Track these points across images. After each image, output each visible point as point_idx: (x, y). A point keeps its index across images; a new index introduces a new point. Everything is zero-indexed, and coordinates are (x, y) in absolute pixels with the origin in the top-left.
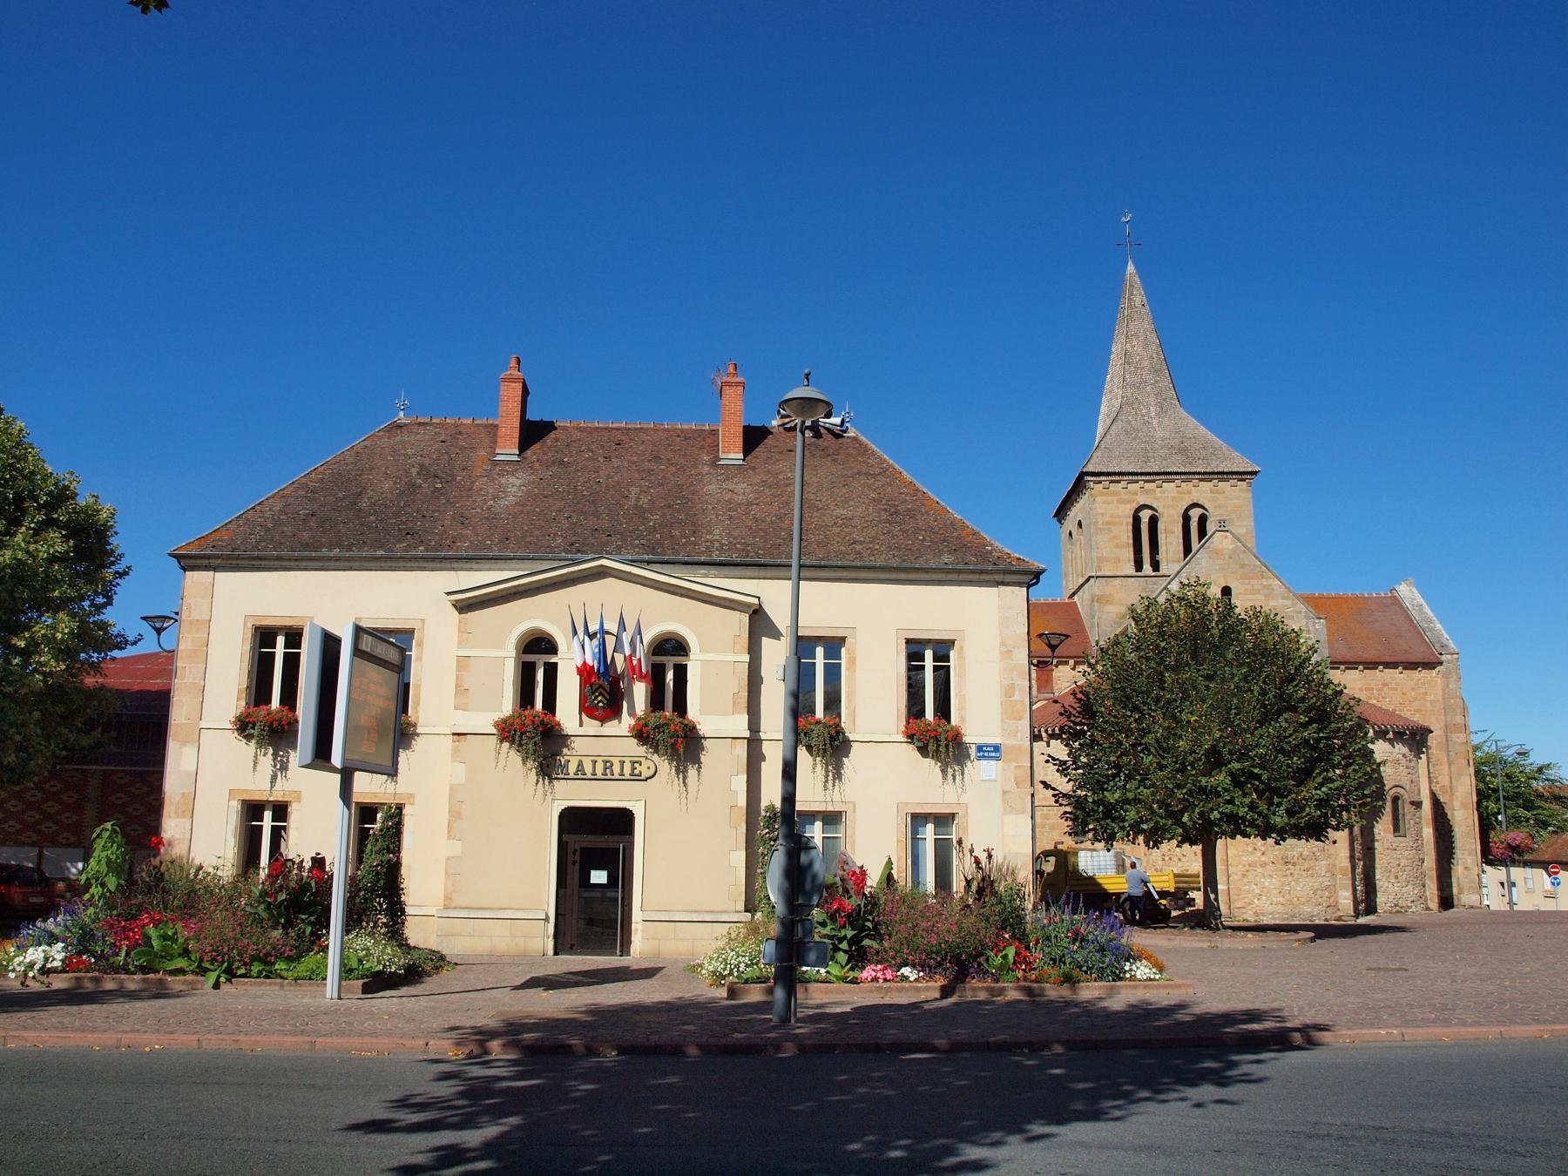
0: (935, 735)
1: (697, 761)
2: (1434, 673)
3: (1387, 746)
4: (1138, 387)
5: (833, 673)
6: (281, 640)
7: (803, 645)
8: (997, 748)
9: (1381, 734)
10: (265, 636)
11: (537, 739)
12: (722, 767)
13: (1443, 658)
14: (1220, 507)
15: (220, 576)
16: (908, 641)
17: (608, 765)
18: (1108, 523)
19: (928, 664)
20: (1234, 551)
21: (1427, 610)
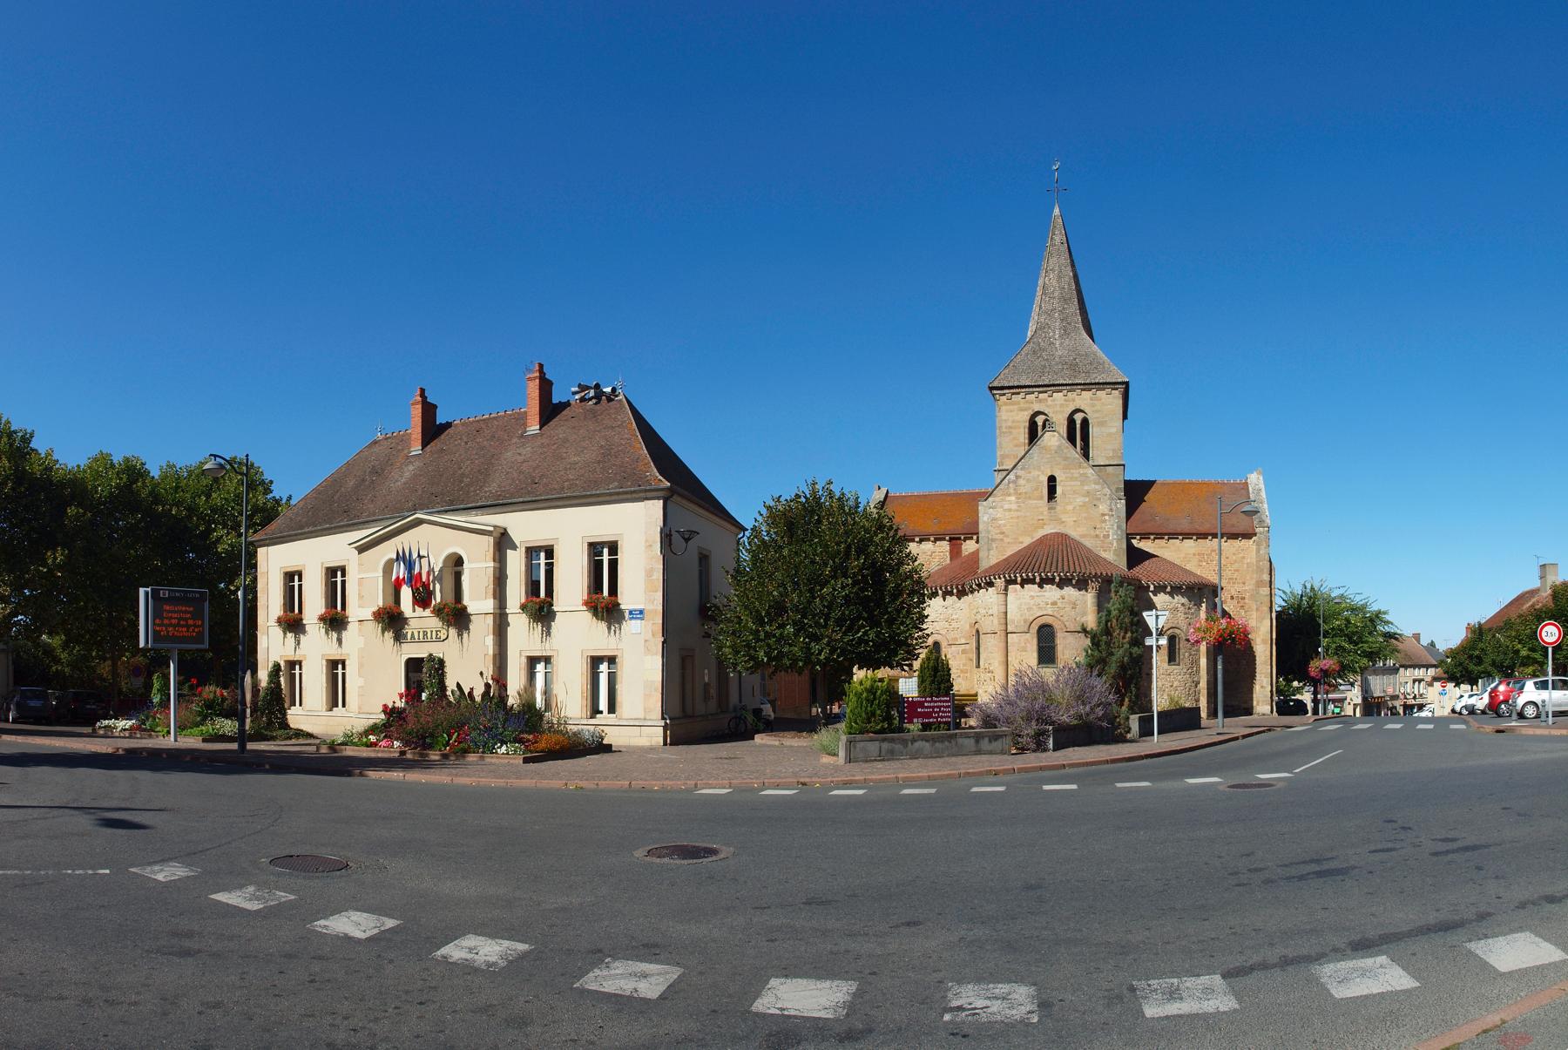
0: (606, 609)
1: (467, 629)
3: (1167, 597)
4: (1049, 314)
5: (614, 565)
6: (606, 551)
7: (531, 552)
8: (641, 612)
9: (1160, 589)
10: (595, 548)
11: (391, 620)
16: (590, 544)
17: (425, 633)
19: (603, 560)
21: (1263, 494)
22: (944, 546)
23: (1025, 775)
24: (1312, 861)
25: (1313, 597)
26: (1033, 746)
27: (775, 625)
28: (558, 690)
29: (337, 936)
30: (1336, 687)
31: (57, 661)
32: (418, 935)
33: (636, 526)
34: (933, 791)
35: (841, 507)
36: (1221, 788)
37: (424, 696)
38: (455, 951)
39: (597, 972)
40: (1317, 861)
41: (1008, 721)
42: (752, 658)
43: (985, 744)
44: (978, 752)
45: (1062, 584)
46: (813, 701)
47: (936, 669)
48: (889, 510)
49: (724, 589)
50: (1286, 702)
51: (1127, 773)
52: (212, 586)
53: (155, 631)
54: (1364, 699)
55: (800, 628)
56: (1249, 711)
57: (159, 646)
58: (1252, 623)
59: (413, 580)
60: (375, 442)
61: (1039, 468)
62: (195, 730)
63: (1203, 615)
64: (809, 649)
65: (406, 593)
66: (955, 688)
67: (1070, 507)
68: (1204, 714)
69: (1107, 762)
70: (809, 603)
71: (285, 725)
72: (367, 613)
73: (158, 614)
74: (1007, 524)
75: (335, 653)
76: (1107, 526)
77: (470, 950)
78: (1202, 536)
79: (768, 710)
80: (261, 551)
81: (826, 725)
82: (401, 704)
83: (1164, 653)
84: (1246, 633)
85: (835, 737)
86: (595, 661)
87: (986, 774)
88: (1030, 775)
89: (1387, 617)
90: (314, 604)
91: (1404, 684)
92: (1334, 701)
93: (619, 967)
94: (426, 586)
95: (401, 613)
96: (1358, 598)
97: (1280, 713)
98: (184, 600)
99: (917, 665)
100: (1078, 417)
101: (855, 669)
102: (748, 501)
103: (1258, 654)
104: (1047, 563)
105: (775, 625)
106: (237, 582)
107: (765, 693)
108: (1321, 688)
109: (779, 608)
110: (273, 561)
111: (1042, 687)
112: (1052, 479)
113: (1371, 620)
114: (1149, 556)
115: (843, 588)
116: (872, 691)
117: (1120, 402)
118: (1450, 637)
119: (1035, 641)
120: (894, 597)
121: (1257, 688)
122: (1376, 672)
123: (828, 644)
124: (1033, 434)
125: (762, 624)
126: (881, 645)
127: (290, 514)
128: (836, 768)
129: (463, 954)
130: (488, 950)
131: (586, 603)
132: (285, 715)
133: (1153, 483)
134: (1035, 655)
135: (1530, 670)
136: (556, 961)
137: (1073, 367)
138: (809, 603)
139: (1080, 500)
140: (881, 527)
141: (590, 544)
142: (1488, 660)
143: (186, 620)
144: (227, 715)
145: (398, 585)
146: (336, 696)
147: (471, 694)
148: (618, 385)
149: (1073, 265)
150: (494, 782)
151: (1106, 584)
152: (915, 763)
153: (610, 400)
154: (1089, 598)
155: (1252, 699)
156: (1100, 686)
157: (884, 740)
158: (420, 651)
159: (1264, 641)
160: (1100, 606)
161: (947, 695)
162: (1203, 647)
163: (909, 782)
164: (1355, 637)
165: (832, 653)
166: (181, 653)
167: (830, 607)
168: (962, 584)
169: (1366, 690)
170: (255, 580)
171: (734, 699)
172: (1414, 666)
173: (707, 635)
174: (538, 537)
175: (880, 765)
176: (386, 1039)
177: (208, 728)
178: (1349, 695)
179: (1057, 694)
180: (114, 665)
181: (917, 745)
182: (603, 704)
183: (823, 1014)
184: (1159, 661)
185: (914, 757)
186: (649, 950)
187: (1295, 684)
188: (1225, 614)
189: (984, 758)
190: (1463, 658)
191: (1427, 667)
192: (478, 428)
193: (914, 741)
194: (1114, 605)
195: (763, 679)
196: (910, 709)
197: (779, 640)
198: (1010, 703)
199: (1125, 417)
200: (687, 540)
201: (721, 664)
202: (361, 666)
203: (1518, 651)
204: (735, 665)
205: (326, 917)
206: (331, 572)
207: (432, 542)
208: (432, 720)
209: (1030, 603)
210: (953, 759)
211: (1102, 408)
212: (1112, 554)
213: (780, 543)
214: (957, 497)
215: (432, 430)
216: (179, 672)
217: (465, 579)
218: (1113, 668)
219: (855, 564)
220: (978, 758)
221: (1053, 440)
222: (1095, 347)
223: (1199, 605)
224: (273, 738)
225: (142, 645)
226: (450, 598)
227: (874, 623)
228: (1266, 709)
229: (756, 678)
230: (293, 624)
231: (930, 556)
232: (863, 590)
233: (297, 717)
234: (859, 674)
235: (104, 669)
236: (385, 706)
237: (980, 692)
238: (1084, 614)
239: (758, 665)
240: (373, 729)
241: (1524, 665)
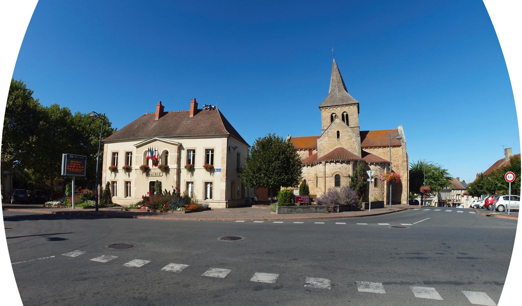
0: (210, 168)
1: (169, 173)
3: (374, 166)
4: (335, 86)
5: (212, 156)
7: (189, 151)
8: (220, 169)
9: (372, 164)
10: (207, 151)
11: (145, 169)
12: (173, 173)
15: (109, 144)
16: (206, 150)
17: (156, 174)
19: (209, 154)
21: (403, 132)
22: (307, 152)
23: (330, 219)
24: (416, 253)
25: (421, 165)
26: (333, 211)
28: (195, 191)
29: (132, 267)
30: (429, 196)
31: (30, 179)
32: (156, 264)
33: (220, 145)
36: (389, 227)
37: (155, 193)
38: (167, 268)
39: (208, 271)
40: (417, 254)
41: (325, 203)
42: (252, 183)
43: (318, 210)
44: (316, 212)
45: (342, 163)
46: (269, 196)
47: (304, 188)
48: (291, 142)
49: (244, 164)
50: (412, 200)
51: (359, 221)
52: (88, 155)
53: (67, 170)
54: (439, 201)
55: (265, 175)
57: (68, 175)
58: (401, 174)
59: (153, 157)
60: (145, 115)
62: (81, 205)
63: (385, 172)
65: (150, 161)
68: (385, 203)
71: (111, 202)
72: (138, 167)
73: (68, 163)
74: (326, 145)
75: (128, 179)
76: (355, 145)
77: (172, 267)
78: (384, 147)
79: (256, 198)
80: (105, 145)
81: (272, 203)
82: (148, 195)
83: (373, 183)
84: (399, 177)
85: (275, 207)
86: (206, 183)
87: (319, 218)
89: (447, 172)
90: (121, 163)
91: (453, 196)
92: (428, 201)
93: (214, 270)
94: (157, 159)
95: (149, 167)
96: (437, 165)
97: (410, 204)
98: (78, 159)
99: (299, 186)
100: (345, 114)
102: (251, 137)
103: (403, 184)
106: (97, 154)
107: (255, 194)
108: (424, 196)
109: (260, 169)
110: (109, 148)
111: (336, 193)
112: (338, 132)
113: (442, 173)
114: (368, 154)
116: (286, 193)
118: (470, 178)
119: (334, 180)
121: (403, 195)
122: (443, 191)
124: (332, 119)
125: (255, 173)
126: (289, 180)
127: (116, 134)
128: (275, 215)
129: (170, 269)
130: (177, 267)
131: (204, 167)
132: (111, 199)
134: (334, 184)
135: (501, 192)
136: (196, 269)
137: (342, 100)
139: (347, 138)
140: (289, 147)
141: (206, 150)
142: (485, 188)
143: (78, 166)
144: (92, 199)
145: (148, 159)
146: (127, 193)
147: (169, 193)
148: (216, 106)
150: (176, 219)
151: (355, 163)
152: (298, 214)
153: (213, 109)
154: (350, 167)
156: (354, 193)
158: (154, 179)
159: (405, 180)
160: (354, 169)
162: (385, 182)
163: (296, 220)
164: (436, 179)
165: (275, 182)
166: (76, 178)
167: (274, 169)
168: (313, 162)
169: (439, 197)
170: (103, 154)
171: (246, 195)
172: (457, 189)
174: (191, 147)
175: (288, 215)
176: (150, 294)
177: (85, 204)
178: (433, 199)
180: (52, 181)
181: (299, 209)
182: (208, 196)
183: (269, 282)
184: (371, 186)
185: (298, 213)
186: (222, 265)
187: (415, 194)
188: (392, 171)
189: (318, 214)
190: (475, 186)
191: (462, 190)
192: (175, 114)
193: (298, 208)
196: (297, 199)
197: (259, 179)
198: (326, 198)
199: (359, 113)
200: (234, 149)
201: (243, 185)
202: (136, 183)
203: (496, 184)
204: (247, 185)
205: (128, 262)
206: (128, 153)
207: (159, 146)
208: (158, 200)
209: (332, 168)
211: (352, 111)
212: (357, 153)
215: (162, 113)
216: (75, 184)
217: (169, 158)
218: (357, 188)
219: (281, 157)
220: (316, 214)
221: (338, 121)
222: (348, 94)
224: (107, 207)
225: (62, 174)
226: (164, 164)
227: (287, 174)
229: (253, 188)
230: (114, 169)
231: (303, 155)
232: (284, 164)
233: (115, 200)
234: (282, 189)
235: (48, 183)
236: (143, 196)
238: (349, 171)
239: (253, 185)
240: (139, 203)
241: (499, 190)
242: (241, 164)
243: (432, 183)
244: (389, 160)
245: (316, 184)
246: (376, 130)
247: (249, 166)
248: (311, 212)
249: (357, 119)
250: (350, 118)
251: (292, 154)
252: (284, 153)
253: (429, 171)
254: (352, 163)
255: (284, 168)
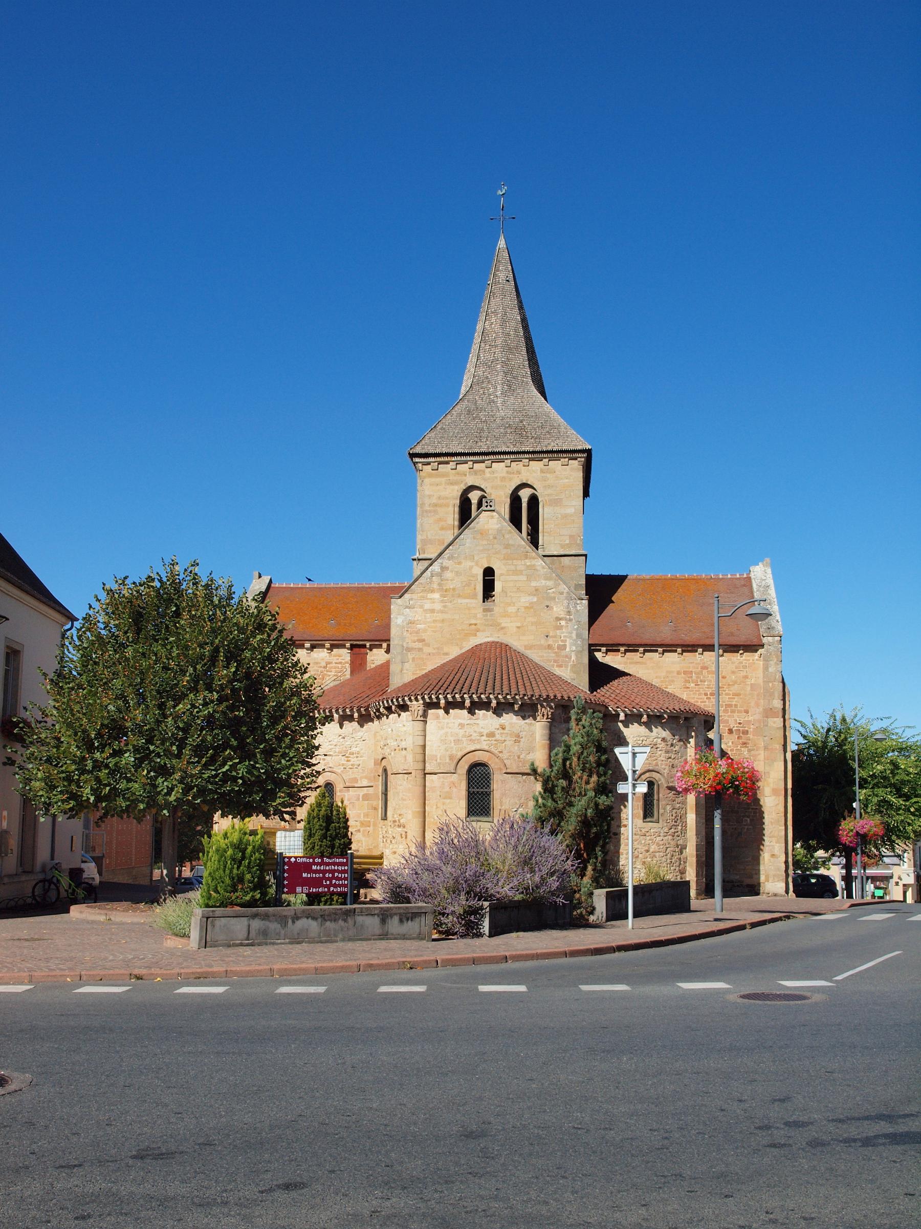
2: (757, 655)
3: (643, 730)
4: (490, 366)
9: (633, 718)
13: (765, 640)
14: (549, 487)
18: (436, 505)
20: (499, 531)
21: (772, 592)
22: (344, 655)
24: (880, 1117)
26: (458, 928)
27: (108, 751)
34: (321, 989)
35: (209, 597)
36: (733, 998)
40: (889, 1118)
41: (425, 894)
42: (73, 796)
43: (394, 925)
44: (384, 936)
45: (501, 709)
46: (157, 856)
47: (328, 819)
48: (271, 603)
55: (143, 756)
56: (753, 889)
58: (759, 766)
61: (472, 558)
64: (155, 786)
66: (353, 846)
67: (512, 609)
68: (693, 893)
69: (565, 954)
70: (158, 722)
74: (428, 628)
76: (563, 633)
78: (690, 648)
79: (91, 871)
81: (173, 893)
85: (184, 911)
87: (400, 968)
88: (460, 970)
92: (874, 879)
96: (908, 733)
100: (525, 494)
101: (217, 816)
104: (481, 683)
105: (108, 751)
107: (88, 847)
109: (116, 729)
111: (475, 844)
112: (489, 572)
114: (617, 674)
115: (205, 704)
116: (240, 847)
117: (580, 475)
119: (464, 785)
120: (275, 720)
121: (765, 857)
123: (181, 781)
124: (465, 514)
125: (90, 748)
128: (187, 956)
133: (626, 577)
137: (520, 431)
138: (158, 722)
139: (525, 600)
140: (260, 627)
149: (521, 307)
151: (561, 712)
154: (536, 730)
155: (758, 872)
156: (556, 848)
157: (254, 916)
159: (775, 792)
160: (553, 742)
161: (343, 854)
162: (691, 798)
163: (287, 976)
165: (186, 791)
167: (185, 730)
168: (369, 704)
171: (43, 854)
173: (10, 762)
175: (248, 951)
178: (896, 871)
179: (495, 859)
181: (301, 923)
184: (630, 814)
185: (296, 940)
187: (820, 853)
188: (723, 754)
189: (393, 944)
193: (296, 918)
194: (575, 736)
195: (86, 826)
196: (290, 873)
197: (112, 773)
199: (586, 493)
209: (456, 733)
210: (350, 945)
211: (557, 484)
212: (572, 674)
213: (122, 639)
214: (363, 593)
218: (571, 825)
219: (223, 673)
220: (383, 944)
221: (492, 522)
222: (547, 407)
223: (685, 741)
227: (245, 753)
228: (780, 887)
229: (77, 824)
232: (232, 708)
234: (222, 824)
237: (387, 853)
238: (531, 750)
242: (25, 698)
243: (890, 805)
244: (707, 705)
245: (380, 804)
246: (658, 573)
247: (65, 709)
248: (360, 936)
249: (579, 520)
250: (545, 512)
251: (271, 659)
252: (233, 655)
253: (877, 756)
254: (544, 712)
255: (234, 725)
